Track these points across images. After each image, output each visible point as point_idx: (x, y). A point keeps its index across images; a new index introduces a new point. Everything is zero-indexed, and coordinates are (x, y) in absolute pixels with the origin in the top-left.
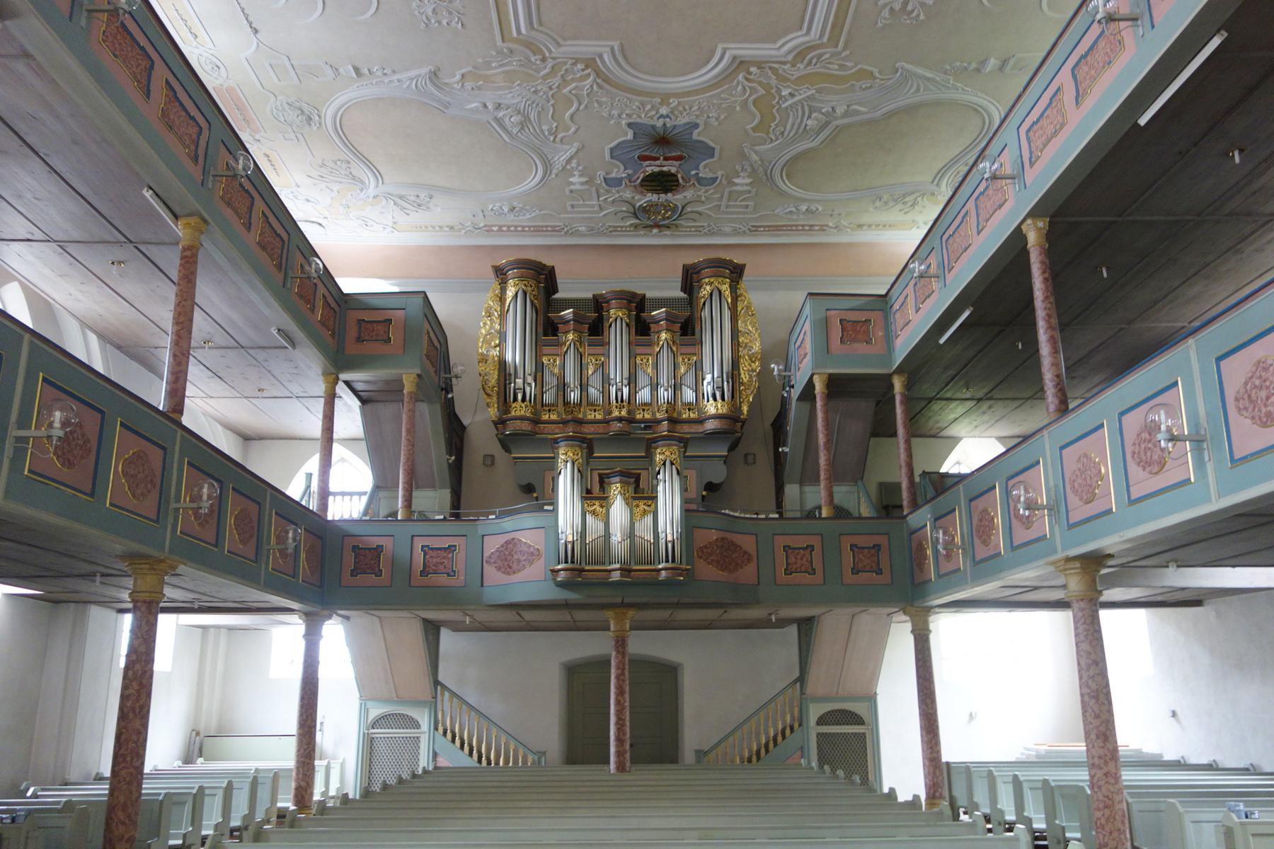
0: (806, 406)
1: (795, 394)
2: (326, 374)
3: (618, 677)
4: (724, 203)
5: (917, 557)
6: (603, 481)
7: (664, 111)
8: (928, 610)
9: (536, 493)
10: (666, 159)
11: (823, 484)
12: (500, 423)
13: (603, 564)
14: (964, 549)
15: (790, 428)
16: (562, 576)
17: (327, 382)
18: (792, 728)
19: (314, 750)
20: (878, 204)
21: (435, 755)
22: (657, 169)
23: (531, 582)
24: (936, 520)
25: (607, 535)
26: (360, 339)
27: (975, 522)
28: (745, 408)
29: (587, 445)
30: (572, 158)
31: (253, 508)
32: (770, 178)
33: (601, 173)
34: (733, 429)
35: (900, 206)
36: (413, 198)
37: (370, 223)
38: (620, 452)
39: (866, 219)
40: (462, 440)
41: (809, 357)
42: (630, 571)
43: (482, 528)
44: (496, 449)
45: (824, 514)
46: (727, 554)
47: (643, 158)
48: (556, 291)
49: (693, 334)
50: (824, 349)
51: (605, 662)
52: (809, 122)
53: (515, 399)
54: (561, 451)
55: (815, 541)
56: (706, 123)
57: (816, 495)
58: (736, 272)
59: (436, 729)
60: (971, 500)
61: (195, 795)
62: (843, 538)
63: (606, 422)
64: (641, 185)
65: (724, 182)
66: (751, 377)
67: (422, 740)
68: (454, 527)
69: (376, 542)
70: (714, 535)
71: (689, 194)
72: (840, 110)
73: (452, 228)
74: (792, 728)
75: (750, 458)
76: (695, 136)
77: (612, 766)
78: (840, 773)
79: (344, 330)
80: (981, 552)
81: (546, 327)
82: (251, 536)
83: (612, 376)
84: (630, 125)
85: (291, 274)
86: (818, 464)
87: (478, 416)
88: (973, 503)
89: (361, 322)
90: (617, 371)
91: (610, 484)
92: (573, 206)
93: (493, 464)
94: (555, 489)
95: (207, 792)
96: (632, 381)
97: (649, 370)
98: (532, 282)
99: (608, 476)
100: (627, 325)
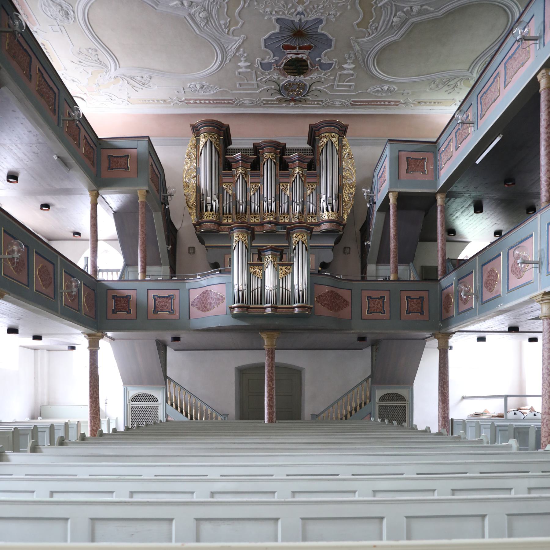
0: (383, 215)
1: (376, 207)
2: (91, 191)
3: (269, 371)
4: (336, 83)
5: (445, 303)
6: (260, 254)
7: (300, 9)
8: (449, 335)
9: (219, 265)
10: (300, 48)
11: (391, 264)
12: (197, 225)
13: (261, 304)
14: (476, 295)
15: (372, 230)
16: (236, 311)
17: (91, 195)
18: (365, 403)
19: (99, 410)
20: (433, 86)
21: (167, 416)
22: (294, 56)
23: (219, 315)
24: (459, 280)
25: (263, 286)
26: (110, 168)
27: (485, 277)
28: (345, 217)
29: (250, 231)
30: (240, 47)
31: (50, 267)
32: (366, 65)
33: (259, 59)
34: (338, 230)
35: (446, 88)
36: (139, 79)
37: (114, 98)
38: (271, 240)
39: (423, 97)
40: (175, 238)
41: (387, 182)
42: (277, 308)
43: (190, 283)
44: (196, 243)
45: (392, 278)
46: (335, 301)
47: (286, 47)
48: (230, 143)
49: (315, 170)
50: (396, 176)
51: (261, 367)
52: (395, 19)
53: (207, 210)
54: (235, 235)
55: (386, 294)
56: (327, 19)
57: (387, 271)
58: (342, 130)
59: (167, 402)
60: (483, 265)
61: (33, 430)
62: (402, 293)
63: (262, 224)
64: (284, 69)
65: (337, 67)
66: (349, 197)
67: (159, 408)
68: (171, 285)
69: (127, 293)
70: (326, 289)
71: (314, 76)
72: (415, 9)
73: (165, 101)
74: (365, 403)
75: (347, 250)
76: (320, 31)
77: (266, 420)
78: (395, 422)
79: (99, 160)
80: (487, 295)
81: (225, 164)
82: (50, 283)
83: (265, 196)
84: (278, 20)
85: (62, 118)
86: (389, 248)
87: (184, 221)
88: (484, 267)
89: (110, 157)
90: (268, 190)
91: (265, 255)
92: (240, 85)
93: (194, 252)
94: (231, 260)
95: (39, 430)
96: (277, 198)
97: (288, 193)
98: (215, 135)
99: (264, 251)
100: (275, 163)
